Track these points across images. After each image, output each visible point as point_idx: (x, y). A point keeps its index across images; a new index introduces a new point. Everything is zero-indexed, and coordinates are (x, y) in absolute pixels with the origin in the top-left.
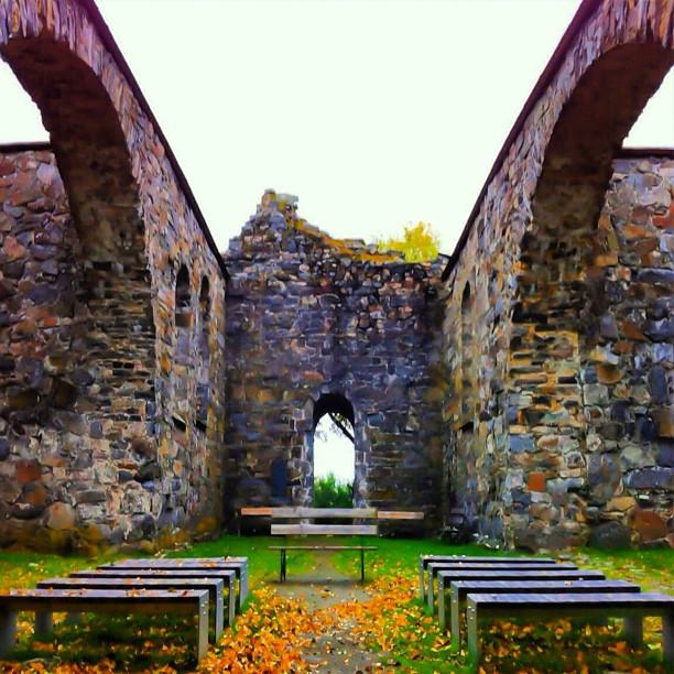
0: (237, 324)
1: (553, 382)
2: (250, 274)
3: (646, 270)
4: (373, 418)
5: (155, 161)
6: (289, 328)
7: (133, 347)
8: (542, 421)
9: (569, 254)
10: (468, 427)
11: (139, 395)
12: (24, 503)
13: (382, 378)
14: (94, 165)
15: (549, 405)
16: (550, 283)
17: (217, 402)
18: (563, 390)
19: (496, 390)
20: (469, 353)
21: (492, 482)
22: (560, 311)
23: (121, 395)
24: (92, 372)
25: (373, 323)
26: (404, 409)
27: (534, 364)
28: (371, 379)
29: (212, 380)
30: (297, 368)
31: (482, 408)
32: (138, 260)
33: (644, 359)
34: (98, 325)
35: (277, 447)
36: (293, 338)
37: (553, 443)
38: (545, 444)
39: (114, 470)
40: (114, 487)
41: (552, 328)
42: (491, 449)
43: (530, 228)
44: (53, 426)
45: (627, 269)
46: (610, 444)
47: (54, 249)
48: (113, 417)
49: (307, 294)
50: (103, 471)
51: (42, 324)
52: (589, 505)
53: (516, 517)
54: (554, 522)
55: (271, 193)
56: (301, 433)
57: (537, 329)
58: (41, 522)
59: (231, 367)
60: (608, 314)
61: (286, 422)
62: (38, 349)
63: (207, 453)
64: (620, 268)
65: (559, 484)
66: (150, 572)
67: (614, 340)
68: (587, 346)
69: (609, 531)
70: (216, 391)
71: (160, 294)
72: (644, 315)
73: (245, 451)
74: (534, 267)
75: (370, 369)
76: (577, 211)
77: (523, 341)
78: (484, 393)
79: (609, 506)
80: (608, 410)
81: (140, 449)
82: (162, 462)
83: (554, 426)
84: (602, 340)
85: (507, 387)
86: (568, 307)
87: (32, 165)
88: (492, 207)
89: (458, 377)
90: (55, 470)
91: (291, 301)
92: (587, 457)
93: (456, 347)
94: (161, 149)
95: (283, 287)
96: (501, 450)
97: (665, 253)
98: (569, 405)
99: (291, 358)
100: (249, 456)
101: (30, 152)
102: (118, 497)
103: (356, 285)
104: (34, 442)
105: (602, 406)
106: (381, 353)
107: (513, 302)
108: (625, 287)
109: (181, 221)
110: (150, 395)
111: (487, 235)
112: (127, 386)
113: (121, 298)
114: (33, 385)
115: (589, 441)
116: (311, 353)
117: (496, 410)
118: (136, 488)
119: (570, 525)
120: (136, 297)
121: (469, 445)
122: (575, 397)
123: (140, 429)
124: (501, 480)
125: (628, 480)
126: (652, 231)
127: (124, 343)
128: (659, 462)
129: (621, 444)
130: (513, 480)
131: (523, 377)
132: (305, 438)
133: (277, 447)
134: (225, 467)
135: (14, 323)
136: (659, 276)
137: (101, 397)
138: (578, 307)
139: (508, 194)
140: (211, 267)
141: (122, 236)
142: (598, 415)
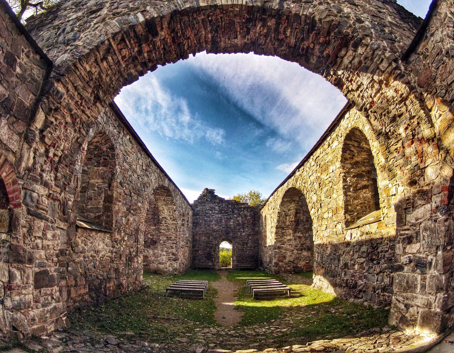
22: (287, 227)
24: (161, 238)
30: (214, 231)
35: (208, 249)
37: (285, 253)
42: (270, 253)
46: (299, 252)
49: (218, 214)
53: (275, 268)
54: (285, 268)
55: (207, 189)
59: (194, 231)
63: (188, 252)
67: (301, 231)
73: (199, 250)
75: (238, 232)
81: (173, 254)
88: (376, 16)
91: (213, 216)
98: (289, 245)
102: (168, 263)
103: (233, 212)
104: (146, 251)
110: (176, 244)
112: (170, 242)
119: (288, 268)
122: (291, 243)
123: (174, 250)
133: (208, 249)
134: (192, 253)
141: (170, 212)
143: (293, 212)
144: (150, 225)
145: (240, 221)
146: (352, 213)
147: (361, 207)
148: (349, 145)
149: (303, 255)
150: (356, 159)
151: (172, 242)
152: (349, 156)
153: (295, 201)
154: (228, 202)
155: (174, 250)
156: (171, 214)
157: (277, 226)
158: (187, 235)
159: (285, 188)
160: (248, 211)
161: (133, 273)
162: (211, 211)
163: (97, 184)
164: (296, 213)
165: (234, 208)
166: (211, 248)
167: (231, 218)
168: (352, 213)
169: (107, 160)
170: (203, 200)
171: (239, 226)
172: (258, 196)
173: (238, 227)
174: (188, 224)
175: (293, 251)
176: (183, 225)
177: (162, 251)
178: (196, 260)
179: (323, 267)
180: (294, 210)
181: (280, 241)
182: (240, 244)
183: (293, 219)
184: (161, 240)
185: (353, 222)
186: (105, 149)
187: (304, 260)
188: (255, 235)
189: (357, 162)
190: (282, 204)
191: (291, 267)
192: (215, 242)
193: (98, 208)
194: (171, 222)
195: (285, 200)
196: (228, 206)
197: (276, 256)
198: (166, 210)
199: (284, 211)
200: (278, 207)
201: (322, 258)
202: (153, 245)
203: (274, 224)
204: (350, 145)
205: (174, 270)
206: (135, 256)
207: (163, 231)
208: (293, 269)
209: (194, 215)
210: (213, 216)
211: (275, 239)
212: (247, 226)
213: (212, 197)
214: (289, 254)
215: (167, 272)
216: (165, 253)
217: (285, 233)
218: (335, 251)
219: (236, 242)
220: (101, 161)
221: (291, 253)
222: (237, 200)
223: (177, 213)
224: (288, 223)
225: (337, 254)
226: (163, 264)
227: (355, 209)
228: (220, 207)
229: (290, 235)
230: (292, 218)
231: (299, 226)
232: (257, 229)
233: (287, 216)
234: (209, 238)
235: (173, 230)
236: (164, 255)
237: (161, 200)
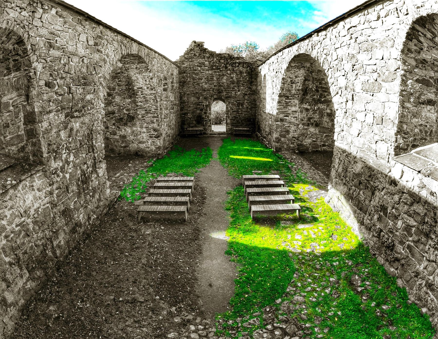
6: (202, 80)
13: (235, 93)
18: (293, 114)
22: (293, 96)
24: (138, 112)
25: (232, 78)
28: (232, 93)
29: (175, 98)
30: (205, 91)
32: (151, 85)
41: (291, 99)
43: (284, 77)
46: (306, 127)
49: (208, 70)
50: (145, 136)
53: (276, 144)
55: (195, 42)
57: (286, 99)
61: (201, 105)
62: (121, 108)
67: (309, 102)
73: (187, 113)
75: (232, 91)
81: (155, 130)
86: (295, 94)
90: (130, 136)
91: (202, 72)
95: (199, 68)
98: (294, 117)
100: (189, 114)
103: (226, 68)
106: (235, 86)
112: (150, 115)
114: (121, 117)
122: (296, 116)
123: (155, 125)
127: (148, 105)
133: (198, 112)
136: (324, 88)
142: (303, 120)
143: (300, 79)
144: (124, 98)
145: (234, 78)
146: (406, 136)
147: (420, 130)
148: (418, 31)
150: (424, 56)
151: (152, 115)
152: (415, 48)
153: (305, 67)
154: (220, 56)
155: (155, 125)
156: (148, 83)
157: (280, 94)
158: (172, 99)
159: (294, 51)
160: (243, 67)
162: (201, 67)
163: (11, 101)
164: (305, 80)
165: (227, 63)
166: (202, 110)
167: (223, 75)
168: (406, 136)
169: (17, 60)
170: (190, 55)
171: (233, 84)
172: (255, 48)
173: (232, 86)
174: (173, 86)
175: (298, 125)
176: (165, 90)
177: (142, 127)
178: (185, 124)
180: (303, 78)
181: (283, 113)
182: (235, 105)
183: (300, 88)
184: (139, 115)
185: (405, 150)
186: (11, 47)
188: (252, 94)
189: (424, 60)
190: (288, 69)
191: (295, 144)
192: (206, 103)
193: (18, 136)
194: (148, 92)
196: (219, 61)
197: (278, 130)
199: (290, 78)
200: (283, 72)
203: (277, 90)
204: (420, 33)
205: (157, 148)
207: (139, 104)
209: (180, 73)
210: (202, 72)
211: (277, 109)
212: (243, 84)
213: (201, 51)
215: (149, 153)
216: (145, 130)
219: (229, 103)
220: (11, 66)
221: (295, 127)
222: (231, 53)
223: (155, 80)
224: (293, 92)
226: (143, 143)
227: (412, 130)
228: (211, 62)
229: (295, 106)
230: (299, 86)
231: (307, 95)
232: (254, 88)
233: (294, 83)
234: (198, 98)
235: (152, 101)
237: (133, 68)
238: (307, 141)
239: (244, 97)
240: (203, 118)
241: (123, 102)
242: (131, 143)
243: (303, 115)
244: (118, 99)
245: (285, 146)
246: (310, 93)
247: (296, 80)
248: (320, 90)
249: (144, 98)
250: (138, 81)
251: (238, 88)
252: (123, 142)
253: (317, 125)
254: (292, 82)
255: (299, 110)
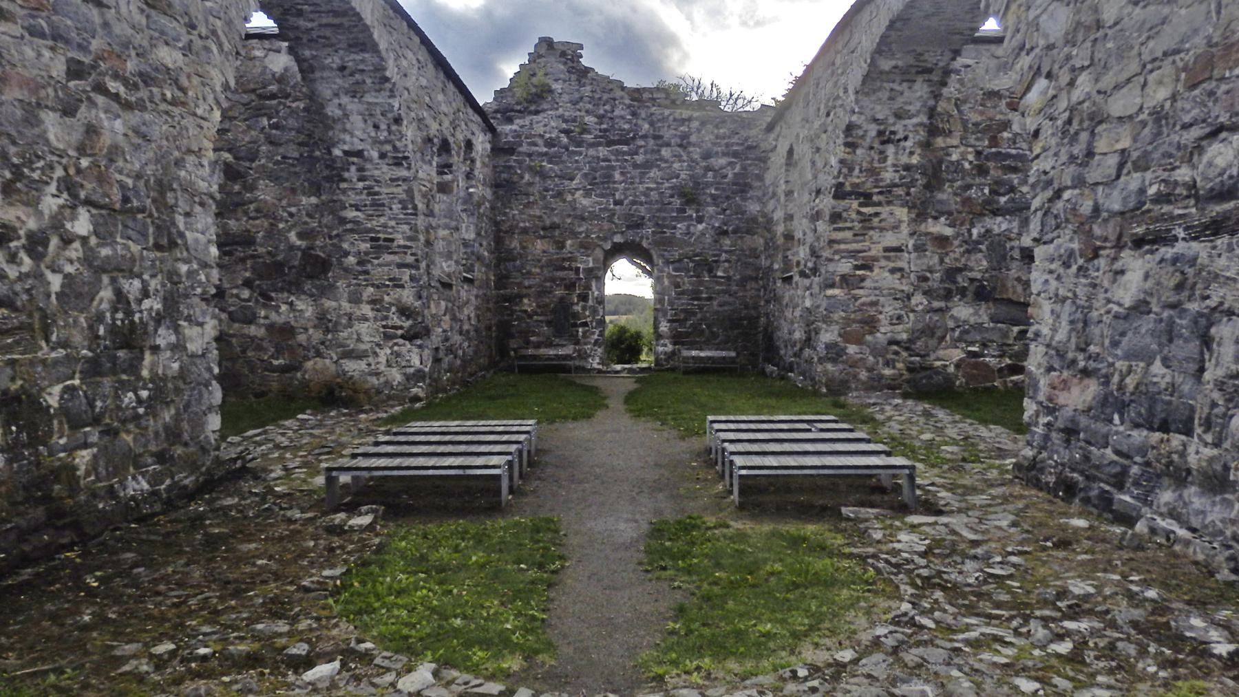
0: (504, 176)
1: (876, 251)
2: (522, 127)
3: (994, 150)
4: (677, 265)
5: (410, 55)
6: (572, 179)
7: (393, 223)
8: (863, 284)
9: (899, 140)
10: (788, 280)
11: (401, 266)
12: (277, 359)
13: (688, 227)
14: (342, 68)
15: (872, 271)
16: (876, 165)
17: (486, 254)
18: (888, 258)
19: (814, 253)
20: (792, 208)
21: (808, 333)
22: (888, 191)
23: (380, 265)
24: (345, 246)
26: (715, 256)
27: (855, 235)
28: (675, 228)
29: (478, 234)
30: (583, 219)
31: (802, 267)
32: (395, 147)
33: (983, 230)
34: (351, 206)
36: (577, 189)
37: (874, 304)
38: (863, 304)
39: (378, 331)
40: (378, 345)
41: (879, 204)
42: (808, 303)
43: (854, 118)
44: (305, 293)
45: (970, 149)
46: (936, 304)
47: (293, 133)
48: (373, 285)
50: (367, 332)
51: (284, 202)
52: (911, 356)
53: (829, 367)
54: (870, 370)
56: (588, 279)
57: (861, 205)
58: (299, 375)
60: (944, 191)
61: (570, 269)
64: (962, 149)
65: (881, 337)
66: (447, 438)
67: (950, 214)
68: (921, 216)
69: (931, 377)
70: (485, 243)
71: (421, 174)
72: (986, 191)
73: (521, 297)
74: (859, 151)
75: (674, 219)
76: (910, 103)
77: (844, 215)
78: (802, 253)
79: (933, 357)
80: (938, 275)
81: (404, 311)
82: (429, 321)
83: (875, 288)
84: (934, 213)
85: (826, 253)
86: (896, 185)
87: (258, 53)
89: (780, 229)
90: (311, 331)
92: (911, 315)
93: (778, 201)
94: (417, 40)
96: (818, 307)
97: (1016, 135)
99: (575, 209)
100: (526, 301)
101: (256, 41)
102: (384, 354)
104: (284, 308)
105: (931, 272)
107: (834, 181)
108: (967, 165)
109: (440, 97)
111: (812, 109)
112: (388, 258)
113: (376, 181)
114: (280, 258)
115: (914, 301)
116: (599, 203)
117: (815, 271)
118: (404, 345)
119: (887, 372)
120: (392, 180)
121: (787, 294)
122: (900, 264)
124: (817, 333)
125: (957, 333)
126: (1002, 113)
127: (382, 220)
128: (993, 319)
129: (950, 305)
130: (828, 336)
131: (842, 247)
132: (594, 284)
133: (559, 292)
135: (251, 202)
136: (1009, 156)
137: (359, 269)
138: (908, 186)
139: (835, 79)
140: (475, 128)
141: (376, 127)
142: (926, 279)
149: (956, 319)
151: (396, 259)
153: (929, 71)
156: (383, 135)
161: (152, 405)
166: (570, 286)
175: (909, 297)
177: (355, 299)
179: (1086, 373)
187: (960, 340)
191: (900, 365)
194: (385, 171)
195: (886, 65)
197: (836, 317)
198: (356, 120)
199: (875, 120)
201: (1082, 324)
202: (310, 277)
205: (408, 378)
206: (159, 319)
208: (907, 375)
214: (890, 308)
216: (366, 310)
217: (876, 220)
218: (1179, 287)
221: (898, 304)
224: (888, 176)
225: (1193, 307)
226: (360, 356)
229: (896, 227)
234: (561, 245)
236: (365, 319)
238: (950, 356)
239: (716, 241)
240: (576, 316)
241: (290, 205)
242: (312, 354)
243: (925, 261)
244: (266, 192)
245: (863, 375)
246: (952, 181)
247: (899, 128)
248: (991, 164)
249: (369, 194)
250: (348, 126)
251: (697, 211)
252: (278, 353)
253: (982, 294)
254: (886, 138)
255: (911, 243)
